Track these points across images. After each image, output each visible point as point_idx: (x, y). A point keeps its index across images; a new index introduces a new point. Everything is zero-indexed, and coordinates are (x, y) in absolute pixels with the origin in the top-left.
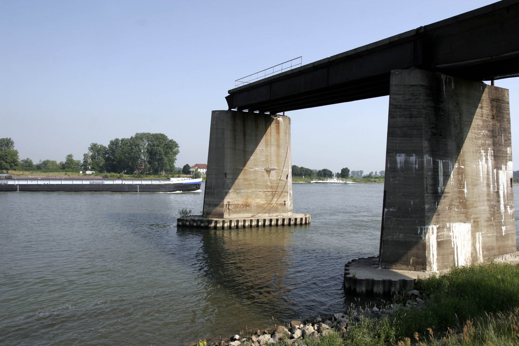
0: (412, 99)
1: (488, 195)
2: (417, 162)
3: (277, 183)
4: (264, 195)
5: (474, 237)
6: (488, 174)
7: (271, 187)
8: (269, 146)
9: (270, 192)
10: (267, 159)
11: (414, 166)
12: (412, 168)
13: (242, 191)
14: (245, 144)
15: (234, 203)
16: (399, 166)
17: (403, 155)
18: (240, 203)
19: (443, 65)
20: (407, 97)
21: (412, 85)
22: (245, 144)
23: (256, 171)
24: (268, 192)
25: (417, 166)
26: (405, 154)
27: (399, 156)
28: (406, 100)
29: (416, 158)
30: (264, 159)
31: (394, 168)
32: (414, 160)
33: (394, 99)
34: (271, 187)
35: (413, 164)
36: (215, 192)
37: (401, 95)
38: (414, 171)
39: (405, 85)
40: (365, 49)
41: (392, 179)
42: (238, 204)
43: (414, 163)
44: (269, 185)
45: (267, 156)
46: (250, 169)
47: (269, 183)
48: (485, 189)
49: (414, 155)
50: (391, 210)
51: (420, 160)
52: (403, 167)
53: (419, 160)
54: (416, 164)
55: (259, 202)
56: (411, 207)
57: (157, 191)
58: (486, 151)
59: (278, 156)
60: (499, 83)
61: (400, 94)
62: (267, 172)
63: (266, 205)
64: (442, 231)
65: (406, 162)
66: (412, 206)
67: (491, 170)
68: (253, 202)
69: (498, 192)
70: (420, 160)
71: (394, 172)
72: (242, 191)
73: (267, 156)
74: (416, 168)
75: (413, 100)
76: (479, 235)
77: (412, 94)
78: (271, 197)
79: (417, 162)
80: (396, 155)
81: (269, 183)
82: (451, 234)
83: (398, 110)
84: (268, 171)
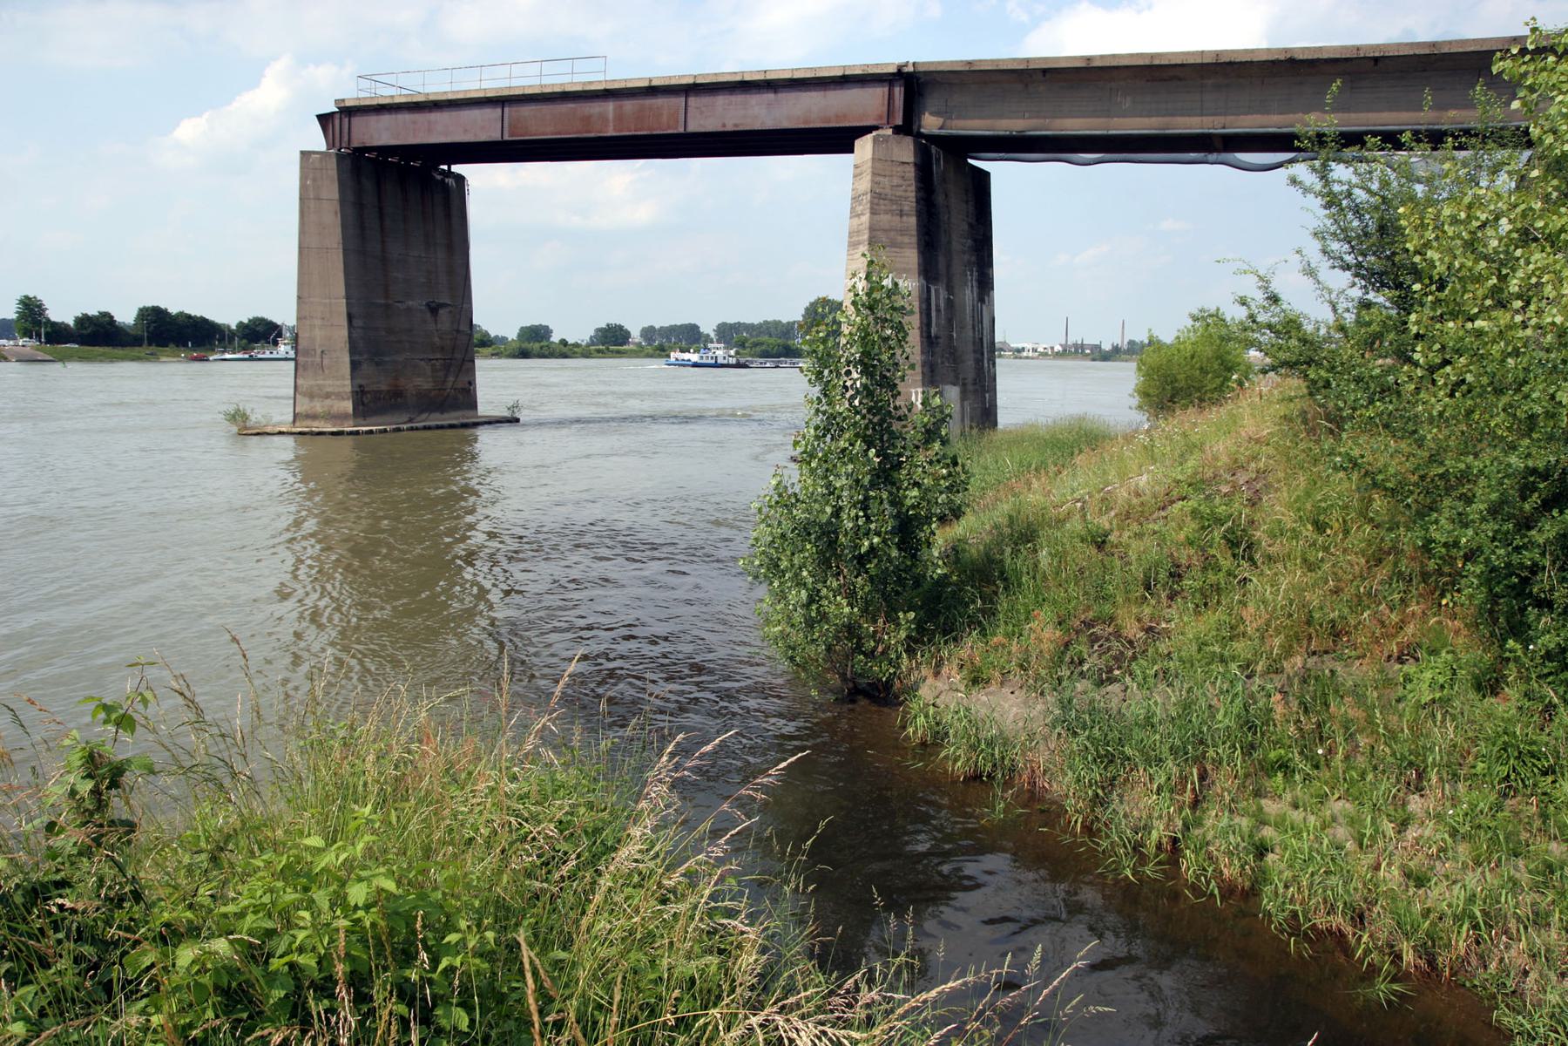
4: (429, 372)
5: (962, 406)
7: (442, 349)
13: (387, 359)
14: (383, 242)
15: (375, 387)
18: (384, 387)
19: (1180, 120)
20: (896, 181)
22: (383, 242)
23: (409, 309)
34: (442, 349)
36: (326, 362)
40: (1147, 62)
42: (380, 392)
47: (436, 339)
48: (971, 334)
58: (972, 271)
60: (456, 168)
63: (433, 393)
69: (981, 339)
72: (387, 359)
76: (966, 403)
78: (441, 374)
81: (436, 339)
84: (434, 309)
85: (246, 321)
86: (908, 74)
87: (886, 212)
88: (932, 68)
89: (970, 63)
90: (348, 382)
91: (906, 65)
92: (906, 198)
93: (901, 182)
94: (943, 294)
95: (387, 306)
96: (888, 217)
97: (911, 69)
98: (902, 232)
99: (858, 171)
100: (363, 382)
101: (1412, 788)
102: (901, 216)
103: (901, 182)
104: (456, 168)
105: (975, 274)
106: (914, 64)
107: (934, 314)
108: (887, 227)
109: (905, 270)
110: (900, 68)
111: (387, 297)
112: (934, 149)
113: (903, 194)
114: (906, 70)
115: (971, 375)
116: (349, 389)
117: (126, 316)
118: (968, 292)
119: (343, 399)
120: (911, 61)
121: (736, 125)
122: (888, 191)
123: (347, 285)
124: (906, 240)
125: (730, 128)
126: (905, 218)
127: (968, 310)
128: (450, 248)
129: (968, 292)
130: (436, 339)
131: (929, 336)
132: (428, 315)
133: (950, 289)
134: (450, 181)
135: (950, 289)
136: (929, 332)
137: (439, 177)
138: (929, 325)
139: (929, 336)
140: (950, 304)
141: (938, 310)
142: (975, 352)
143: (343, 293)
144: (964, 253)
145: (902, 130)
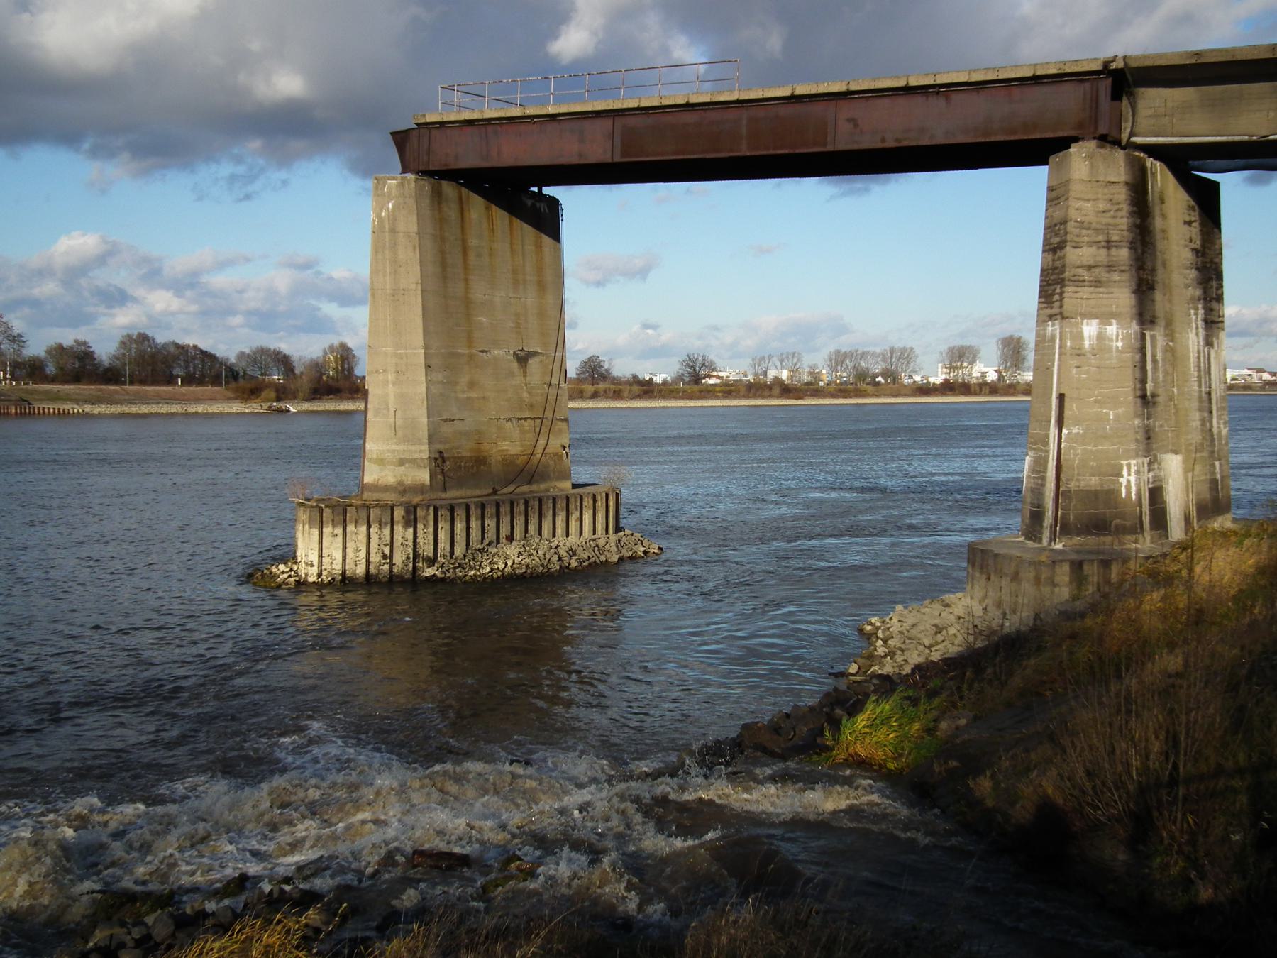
0: (1110, 211)
1: (1200, 397)
2: (1120, 337)
3: (542, 395)
6: (1199, 352)
8: (521, 287)
9: (529, 420)
10: (518, 325)
11: (1114, 344)
12: (1110, 348)
14: (466, 280)
16: (1087, 344)
17: (1095, 322)
19: (1148, 139)
20: (1102, 206)
21: (1109, 182)
24: (525, 419)
25: (1120, 344)
26: (1097, 321)
27: (1087, 324)
28: (1099, 212)
29: (1118, 328)
30: (512, 325)
31: (1079, 349)
32: (1115, 333)
33: (1077, 209)
34: (531, 406)
35: (1112, 339)
37: (1091, 202)
38: (1114, 354)
39: (1097, 181)
41: (1075, 369)
43: (1114, 338)
44: (527, 400)
45: (517, 315)
46: (481, 354)
48: (1196, 388)
49: (1114, 321)
50: (1075, 431)
51: (1125, 332)
52: (1095, 347)
53: (1122, 333)
54: (1117, 341)
55: (507, 450)
56: (1109, 425)
57: (747, 408)
58: (1196, 309)
59: (542, 314)
60: (547, 190)
61: (1088, 200)
62: (521, 363)
64: (554, 593)
65: (1101, 337)
66: (1111, 422)
67: (1201, 348)
68: (494, 450)
69: (1209, 394)
70: (1125, 332)
71: (1079, 355)
73: (517, 315)
74: (1117, 347)
75: (1112, 212)
77: (1111, 200)
79: (1120, 337)
80: (1082, 323)
82: (1162, 474)
83: (1084, 232)
84: (523, 359)
85: (247, 351)
86: (1117, 71)
87: (1090, 244)
88: (1148, 63)
89: (1198, 54)
90: (425, 447)
91: (1114, 59)
92: (1116, 225)
93: (1108, 206)
94: (1161, 341)
95: (471, 357)
96: (1093, 250)
97: (1119, 64)
98: (1110, 267)
99: (1054, 194)
100: (441, 447)
101: (271, 835)
102: (1108, 248)
103: (1108, 206)
104: (547, 190)
105: (1201, 311)
106: (1125, 58)
107: (1149, 366)
108: (1091, 263)
109: (1113, 315)
110: (1106, 64)
111: (470, 347)
112: (1149, 162)
113: (1111, 221)
114: (1113, 66)
115: (1196, 437)
116: (425, 455)
117: (105, 349)
118: (1192, 336)
119: (419, 466)
120: (1121, 54)
121: (898, 140)
122: (1091, 218)
123: (426, 332)
124: (1116, 277)
125: (891, 144)
126: (1114, 252)
127: (1192, 360)
128: (541, 286)
129: (1192, 336)
130: (525, 394)
131: (1144, 397)
132: (515, 365)
133: (1170, 335)
134: (543, 207)
135: (1170, 335)
136: (1144, 389)
137: (529, 202)
138: (1143, 381)
139: (1144, 397)
140: (1170, 351)
141: (1154, 361)
142: (1200, 410)
143: (421, 343)
144: (1187, 286)
145: (1109, 140)
